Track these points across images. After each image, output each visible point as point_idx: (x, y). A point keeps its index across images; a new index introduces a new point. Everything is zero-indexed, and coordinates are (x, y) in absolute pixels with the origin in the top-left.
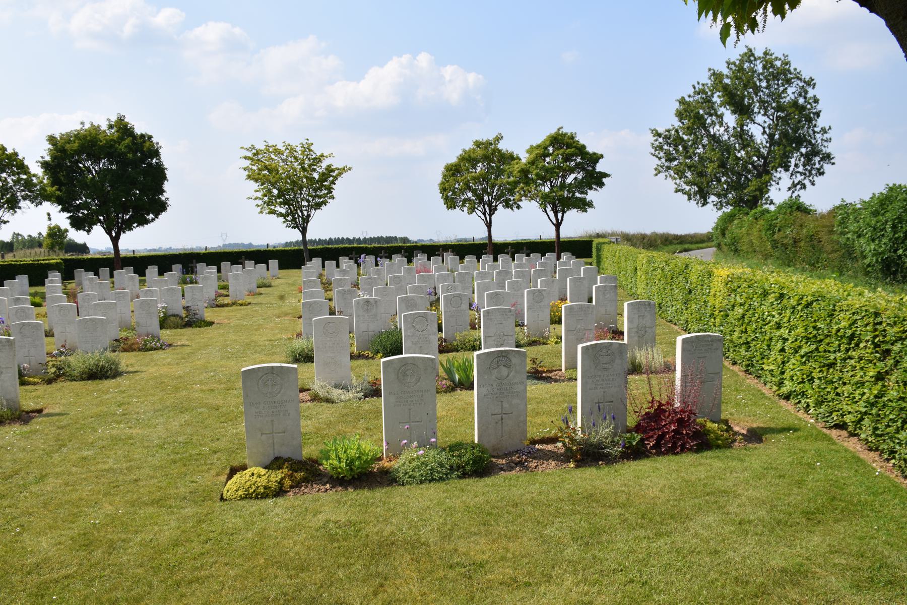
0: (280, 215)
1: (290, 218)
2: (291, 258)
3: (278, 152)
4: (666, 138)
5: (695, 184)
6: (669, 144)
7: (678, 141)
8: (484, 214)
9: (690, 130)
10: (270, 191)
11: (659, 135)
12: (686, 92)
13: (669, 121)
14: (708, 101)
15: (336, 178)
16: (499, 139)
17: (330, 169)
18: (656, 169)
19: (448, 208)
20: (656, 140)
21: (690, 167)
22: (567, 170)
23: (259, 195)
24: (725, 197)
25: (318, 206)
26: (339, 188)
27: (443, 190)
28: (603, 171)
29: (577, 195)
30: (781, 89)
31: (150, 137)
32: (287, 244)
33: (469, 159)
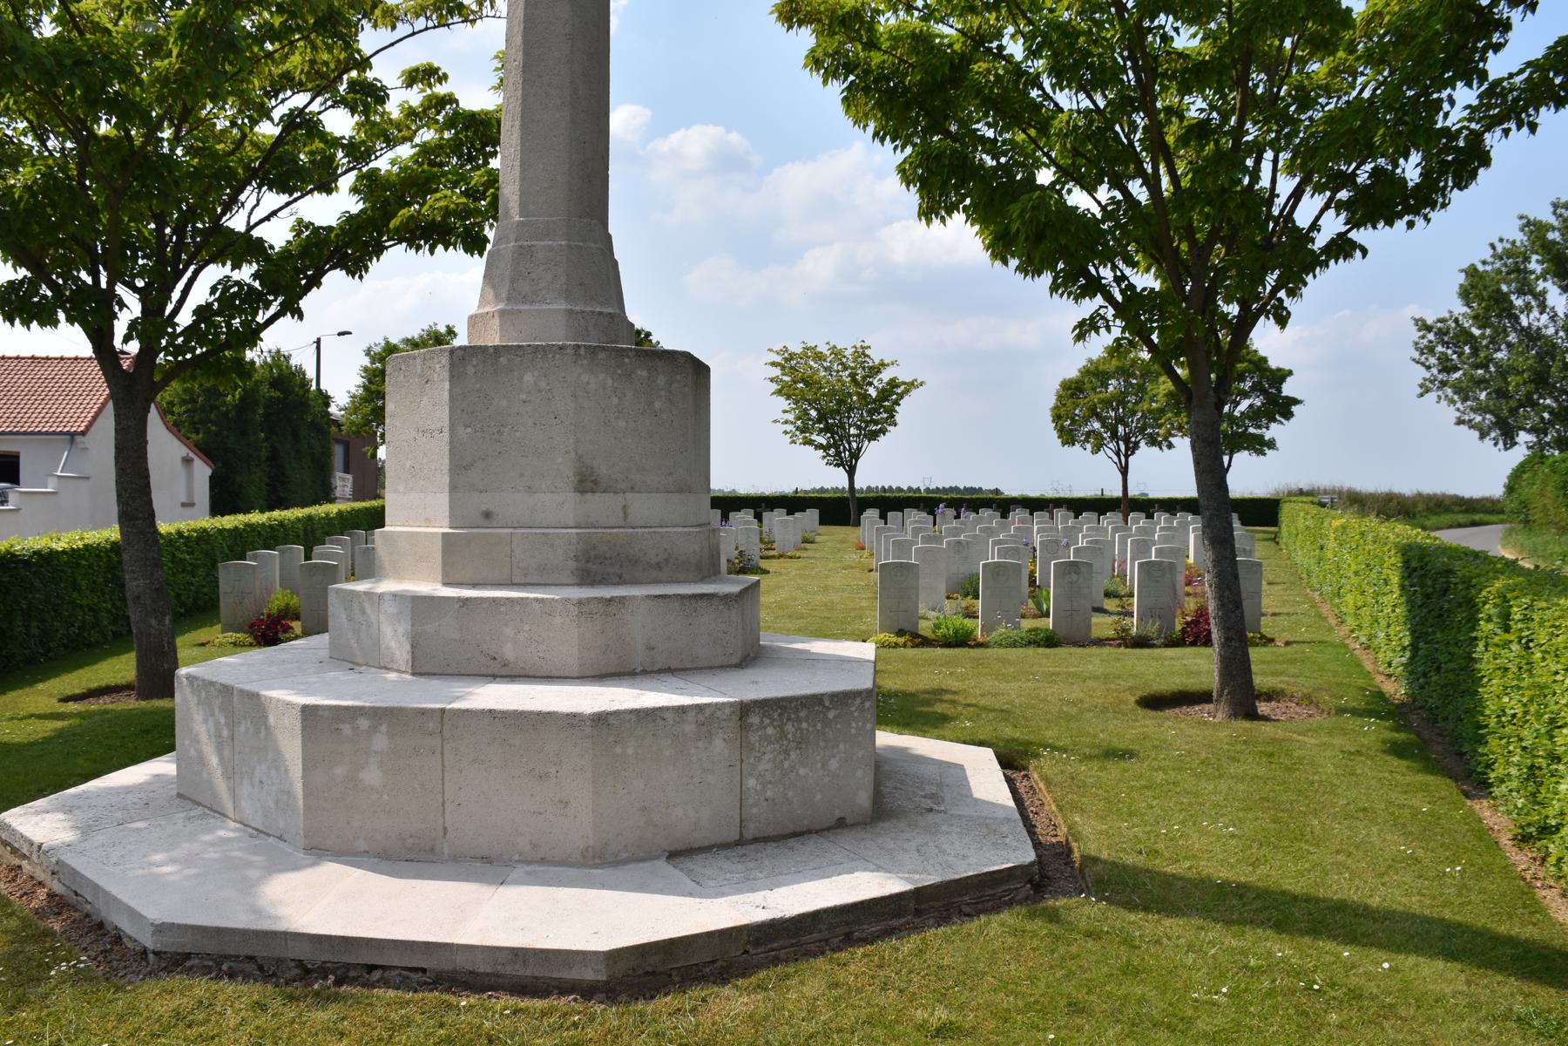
0: (819, 447)
1: (832, 452)
2: (838, 510)
3: (819, 357)
4: (1441, 333)
5: (1491, 412)
6: (1446, 344)
7: (1464, 336)
10: (806, 412)
11: (1429, 329)
13: (1448, 304)
15: (901, 396)
17: (893, 383)
18: (1421, 386)
19: (1063, 444)
20: (1423, 337)
23: (791, 417)
25: (873, 436)
26: (904, 411)
27: (1057, 418)
28: (1291, 395)
29: (1251, 430)
31: (648, 334)
32: (814, 491)
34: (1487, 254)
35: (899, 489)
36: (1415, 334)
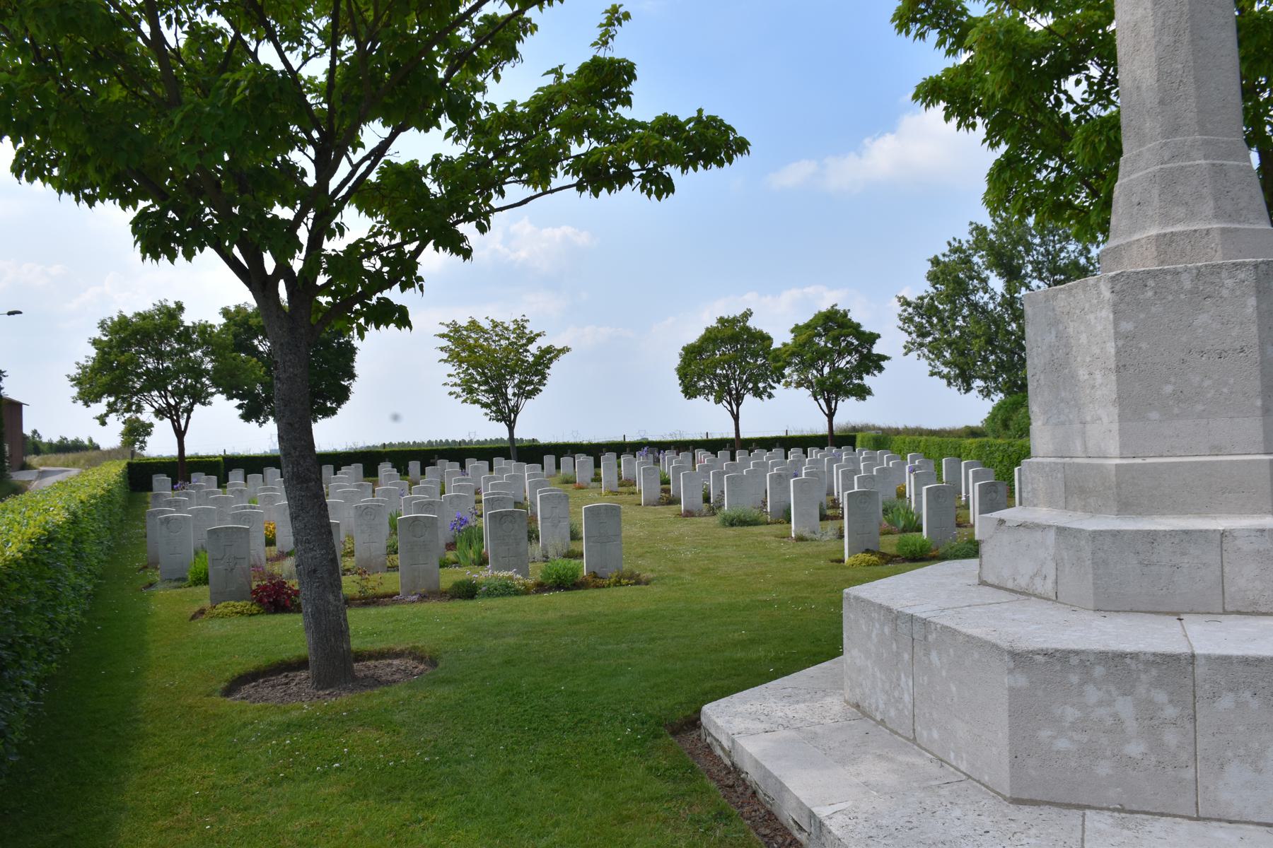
0: (484, 405)
5: (956, 366)
6: (921, 316)
8: (730, 404)
9: (950, 299)
12: (941, 249)
14: (967, 261)
16: (747, 315)
17: (549, 350)
21: (949, 345)
22: (835, 352)
24: (995, 380)
25: (530, 395)
26: (555, 371)
30: (1058, 246)
33: (711, 338)
34: (946, 250)
35: (419, 445)
36: (899, 309)
